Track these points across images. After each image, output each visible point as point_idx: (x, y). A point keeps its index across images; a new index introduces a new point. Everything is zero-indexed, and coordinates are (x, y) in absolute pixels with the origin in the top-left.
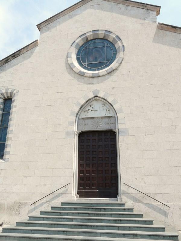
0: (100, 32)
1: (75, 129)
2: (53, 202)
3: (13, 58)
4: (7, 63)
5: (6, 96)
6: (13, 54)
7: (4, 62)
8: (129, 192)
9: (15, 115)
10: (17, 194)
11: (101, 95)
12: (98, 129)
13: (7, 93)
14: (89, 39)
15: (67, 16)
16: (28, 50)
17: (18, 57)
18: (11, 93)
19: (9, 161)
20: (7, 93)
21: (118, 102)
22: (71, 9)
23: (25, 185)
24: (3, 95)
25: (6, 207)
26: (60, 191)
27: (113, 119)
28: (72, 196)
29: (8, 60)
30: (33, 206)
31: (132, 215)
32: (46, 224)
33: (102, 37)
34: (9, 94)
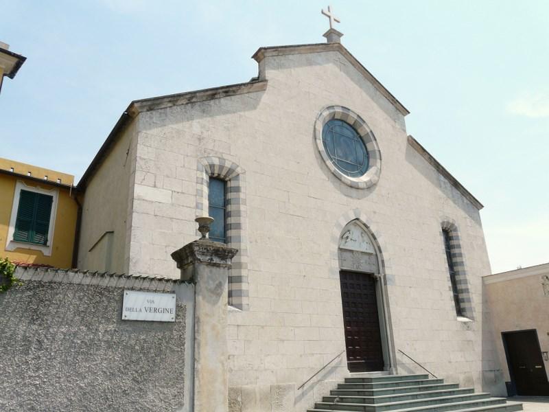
0: (351, 114)
1: (336, 266)
2: (326, 381)
3: (224, 94)
4: (212, 99)
5: (216, 172)
6: (228, 87)
7: (209, 96)
8: (404, 362)
9: (247, 219)
10: (272, 372)
11: (363, 219)
12: (359, 270)
13: (221, 167)
14: (336, 118)
15: (304, 57)
16: (251, 90)
17: (233, 97)
18: (230, 171)
19: (249, 309)
20: (221, 167)
21: (381, 235)
22: (310, 49)
23: (283, 355)
24: (212, 168)
25: (258, 396)
26: (333, 364)
27: (376, 255)
28: (344, 373)
29: (215, 94)
30: (300, 391)
31: (443, 386)
32: (406, 404)
33: (352, 123)
34: (215, 168)
